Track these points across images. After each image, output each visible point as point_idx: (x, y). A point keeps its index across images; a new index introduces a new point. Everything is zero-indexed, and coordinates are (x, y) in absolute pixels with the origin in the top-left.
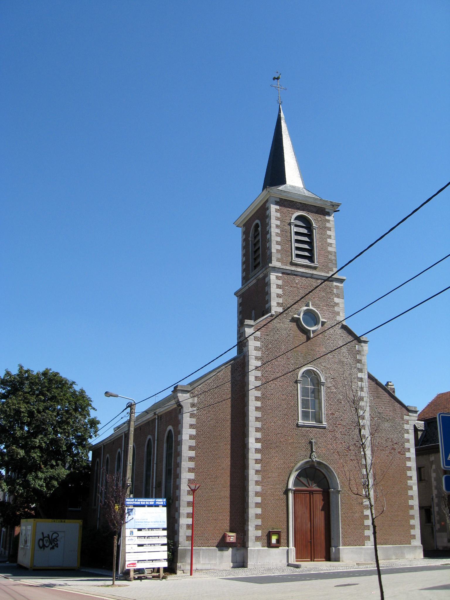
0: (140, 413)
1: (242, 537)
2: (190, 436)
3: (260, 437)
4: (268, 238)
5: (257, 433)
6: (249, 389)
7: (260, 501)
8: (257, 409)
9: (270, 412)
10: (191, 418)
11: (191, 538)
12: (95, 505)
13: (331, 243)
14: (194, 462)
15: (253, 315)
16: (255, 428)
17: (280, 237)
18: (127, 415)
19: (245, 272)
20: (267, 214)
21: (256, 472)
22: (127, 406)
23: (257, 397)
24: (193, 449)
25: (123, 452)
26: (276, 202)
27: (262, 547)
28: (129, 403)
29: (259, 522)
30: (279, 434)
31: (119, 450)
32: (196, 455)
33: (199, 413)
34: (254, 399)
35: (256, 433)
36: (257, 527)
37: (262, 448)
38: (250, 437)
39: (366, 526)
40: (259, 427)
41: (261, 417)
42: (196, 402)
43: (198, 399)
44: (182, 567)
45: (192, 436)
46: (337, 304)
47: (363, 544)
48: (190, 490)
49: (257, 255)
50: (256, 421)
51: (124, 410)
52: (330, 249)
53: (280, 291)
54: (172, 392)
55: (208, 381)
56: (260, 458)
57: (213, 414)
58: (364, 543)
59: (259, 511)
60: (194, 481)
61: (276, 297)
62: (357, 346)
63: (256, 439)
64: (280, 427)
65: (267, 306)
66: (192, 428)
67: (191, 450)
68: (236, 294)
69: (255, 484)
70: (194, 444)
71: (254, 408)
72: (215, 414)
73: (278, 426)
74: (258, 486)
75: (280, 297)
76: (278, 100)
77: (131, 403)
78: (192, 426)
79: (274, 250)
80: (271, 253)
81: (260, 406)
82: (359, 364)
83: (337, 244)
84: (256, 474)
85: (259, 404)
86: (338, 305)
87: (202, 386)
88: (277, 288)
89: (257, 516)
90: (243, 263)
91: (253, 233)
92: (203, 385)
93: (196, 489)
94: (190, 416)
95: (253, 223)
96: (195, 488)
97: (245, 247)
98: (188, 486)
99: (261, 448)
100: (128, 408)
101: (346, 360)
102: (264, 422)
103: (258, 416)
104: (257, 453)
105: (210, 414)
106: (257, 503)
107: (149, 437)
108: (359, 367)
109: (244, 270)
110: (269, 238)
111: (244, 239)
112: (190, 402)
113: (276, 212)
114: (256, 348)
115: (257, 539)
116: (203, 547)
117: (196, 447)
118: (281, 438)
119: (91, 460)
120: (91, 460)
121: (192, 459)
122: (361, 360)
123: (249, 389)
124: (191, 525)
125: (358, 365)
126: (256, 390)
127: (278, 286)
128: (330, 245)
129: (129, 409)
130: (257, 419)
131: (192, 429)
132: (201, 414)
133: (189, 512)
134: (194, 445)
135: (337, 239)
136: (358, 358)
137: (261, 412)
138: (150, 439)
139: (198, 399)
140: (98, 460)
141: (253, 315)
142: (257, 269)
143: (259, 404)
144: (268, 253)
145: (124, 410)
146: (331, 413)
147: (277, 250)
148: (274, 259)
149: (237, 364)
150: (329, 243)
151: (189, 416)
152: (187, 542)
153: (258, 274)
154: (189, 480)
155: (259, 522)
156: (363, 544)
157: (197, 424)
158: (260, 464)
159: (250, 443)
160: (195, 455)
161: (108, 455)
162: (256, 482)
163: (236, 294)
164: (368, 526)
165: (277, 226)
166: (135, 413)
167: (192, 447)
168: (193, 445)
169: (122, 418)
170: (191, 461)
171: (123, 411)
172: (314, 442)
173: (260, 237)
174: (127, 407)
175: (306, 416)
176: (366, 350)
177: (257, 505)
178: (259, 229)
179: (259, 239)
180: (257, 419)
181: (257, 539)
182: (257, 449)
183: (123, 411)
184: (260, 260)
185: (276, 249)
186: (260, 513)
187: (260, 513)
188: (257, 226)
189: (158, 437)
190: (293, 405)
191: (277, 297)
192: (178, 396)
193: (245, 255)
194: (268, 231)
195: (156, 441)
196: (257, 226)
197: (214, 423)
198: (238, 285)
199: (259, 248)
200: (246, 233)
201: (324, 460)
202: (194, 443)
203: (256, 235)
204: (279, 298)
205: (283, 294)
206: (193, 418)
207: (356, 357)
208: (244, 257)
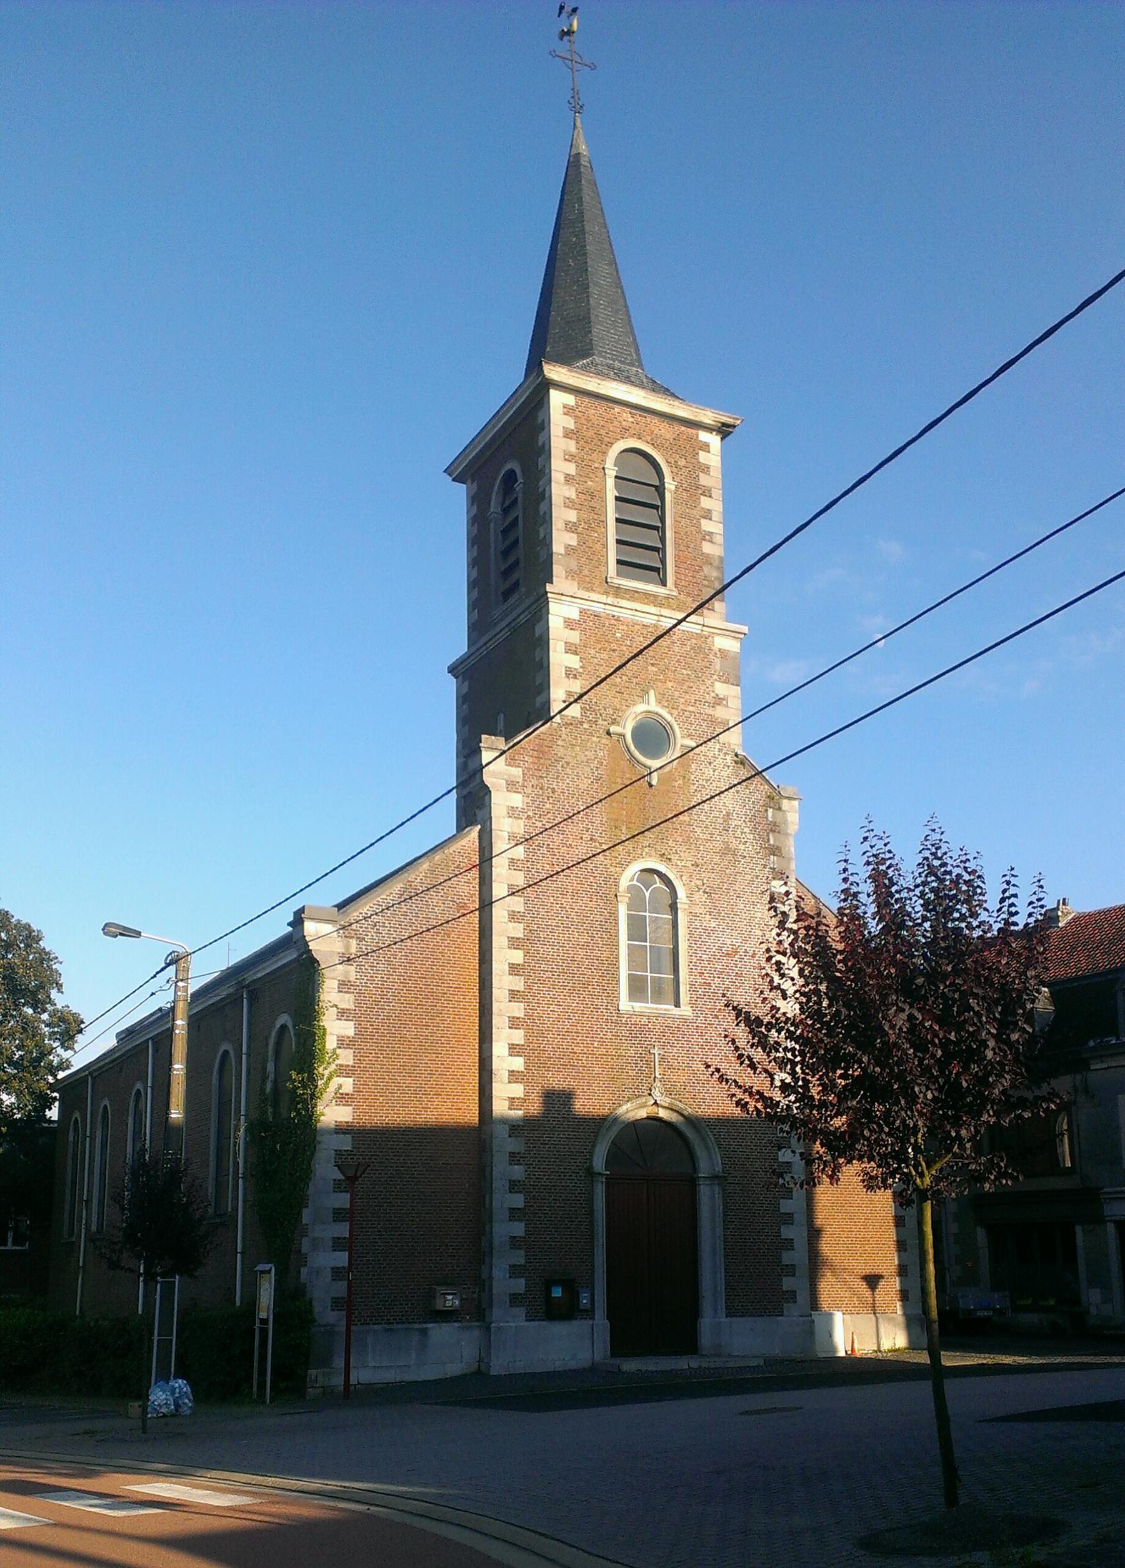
0: (217, 974)
1: (475, 1296)
2: (338, 1040)
3: (522, 1042)
4: (542, 513)
5: (514, 1030)
6: (493, 900)
7: (521, 1205)
8: (514, 969)
9: (547, 978)
10: (341, 992)
11: (344, 1304)
12: (71, 1234)
13: (712, 533)
14: (351, 1105)
15: (501, 725)
16: (509, 1017)
17: (575, 511)
18: (169, 985)
19: (476, 610)
20: (540, 444)
21: (510, 1130)
22: (168, 961)
23: (512, 938)
24: (346, 1073)
25: (149, 1089)
26: (564, 407)
27: (527, 1320)
28: (171, 954)
29: (519, 1258)
30: (570, 1034)
31: (139, 1086)
32: (356, 1089)
33: (363, 979)
34: (505, 1051)
35: (510, 1030)
36: (515, 1271)
37: (526, 1069)
38: (496, 1082)
39: (787, 1265)
40: (518, 1016)
41: (522, 989)
42: (353, 950)
43: (358, 944)
44: (320, 1379)
45: (346, 1039)
46: (721, 699)
47: (779, 1312)
48: (343, 1178)
49: (512, 559)
50: (510, 1001)
51: (158, 973)
52: (707, 548)
53: (574, 661)
54: (289, 924)
55: (385, 897)
56: (522, 1096)
57: (399, 981)
58: (781, 1309)
59: (519, 1229)
60: (351, 1155)
61: (564, 675)
62: (771, 810)
63: (511, 1046)
64: (571, 1015)
65: (539, 700)
66: (343, 1018)
67: (343, 1076)
68: (452, 670)
69: (509, 1160)
70: (349, 1061)
71: (507, 967)
72: (403, 983)
73: (567, 1012)
74: (516, 1167)
75: (575, 677)
76: (572, 101)
77: (176, 954)
78: (344, 1013)
79: (558, 548)
80: (550, 555)
81: (522, 962)
82: (775, 857)
83: (725, 535)
84: (510, 1136)
85: (518, 957)
86: (725, 702)
87: (368, 910)
88: (566, 652)
89: (514, 1242)
90: (472, 585)
91: (501, 499)
92: (370, 907)
93: (358, 1174)
94: (339, 988)
95: (500, 470)
96: (356, 1174)
97: (477, 540)
98: (336, 1168)
99: (523, 1070)
100: (171, 967)
101: (742, 847)
102: (532, 1003)
103: (517, 989)
104: (515, 1082)
105: (390, 982)
106: (513, 1209)
107: (225, 1046)
108: (775, 867)
109: (473, 605)
110: (545, 513)
111: (475, 516)
112: (339, 950)
113: (566, 436)
114: (513, 812)
115: (515, 1299)
116: (374, 1324)
117: (355, 1067)
118: (573, 1043)
119: (56, 1119)
120: (56, 1119)
121: (345, 1098)
122: (778, 848)
123: (493, 900)
124: (344, 1268)
125: (772, 860)
126: (510, 921)
127: (571, 649)
128: (708, 536)
129: (173, 968)
130: (514, 995)
131: (345, 1022)
132: (369, 982)
133: (336, 1235)
134: (351, 1063)
135: (726, 521)
136: (772, 842)
137: (522, 1004)
138: (226, 1052)
139: (358, 944)
140: (77, 1115)
141: (501, 725)
142: (511, 601)
143: (518, 957)
144: (543, 555)
145: (158, 973)
146: (703, 981)
147: (568, 547)
148: (558, 570)
149: (460, 852)
150: (705, 531)
151: (336, 987)
152: (334, 1313)
153: (515, 614)
154: (339, 1153)
155: (519, 1258)
156: (779, 1312)
157: (357, 1009)
158: (521, 1109)
159: (494, 1058)
160: (354, 1088)
161: (106, 1102)
162: (512, 1155)
163: (452, 670)
164: (792, 1265)
165: (568, 479)
166: (188, 979)
167: (344, 1068)
168: (347, 1063)
169: (153, 994)
170: (344, 1105)
171: (155, 976)
172: (659, 1054)
173: (518, 511)
174: (168, 965)
175: (637, 988)
176: (793, 823)
177: (514, 1214)
178: (518, 487)
179: (518, 537)
180: (514, 995)
181: (515, 1299)
182: (513, 1071)
183: (155, 976)
184: (521, 552)
185: (565, 544)
186: (522, 1234)
187: (522, 1234)
188: (511, 476)
189: (249, 1047)
190: (607, 960)
191: (568, 676)
192: (305, 936)
193: (477, 562)
194: (541, 493)
195: (244, 1057)
196: (511, 476)
197: (402, 1005)
198: (458, 646)
199: (516, 541)
200: (478, 501)
201: (683, 1100)
202: (352, 1057)
203: (507, 503)
204: (571, 680)
205: (581, 667)
206: (345, 992)
207: (768, 840)
208: (473, 568)
